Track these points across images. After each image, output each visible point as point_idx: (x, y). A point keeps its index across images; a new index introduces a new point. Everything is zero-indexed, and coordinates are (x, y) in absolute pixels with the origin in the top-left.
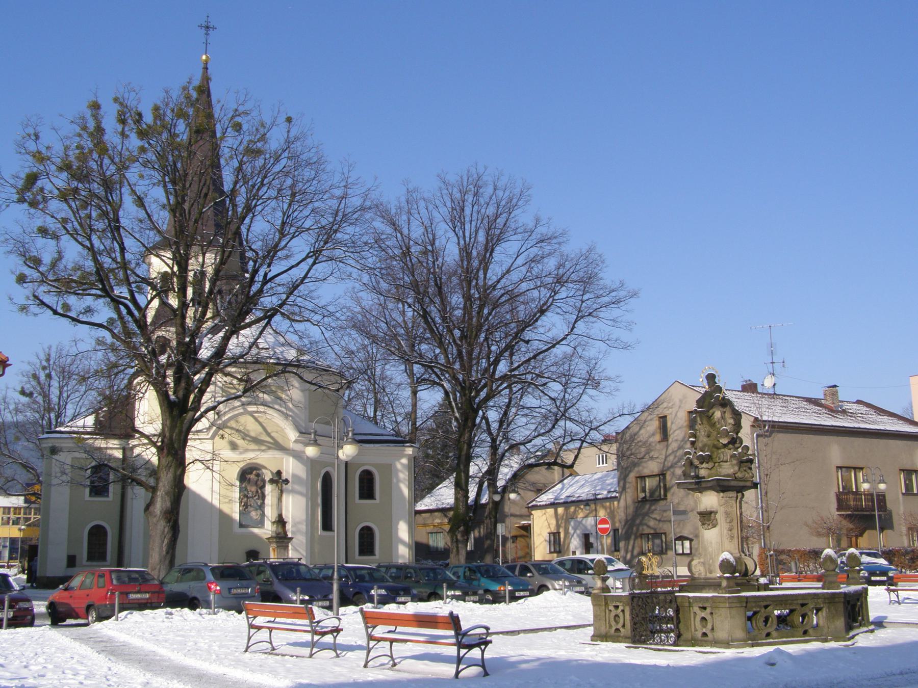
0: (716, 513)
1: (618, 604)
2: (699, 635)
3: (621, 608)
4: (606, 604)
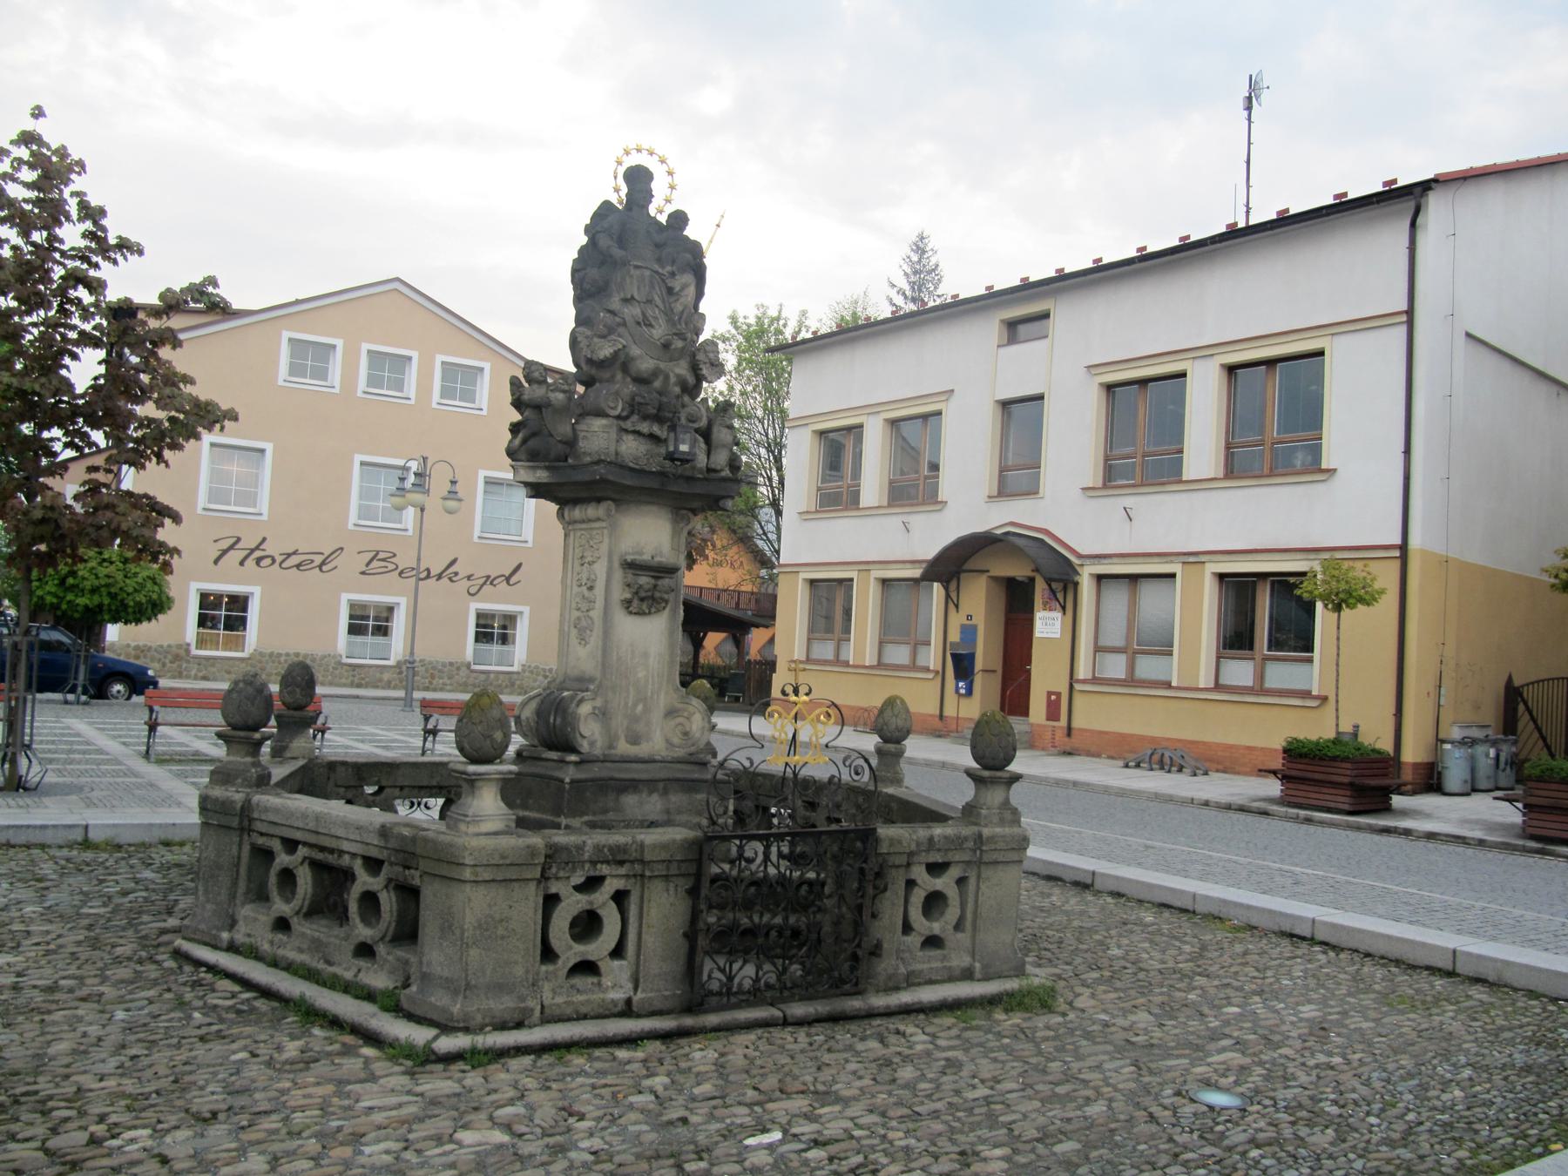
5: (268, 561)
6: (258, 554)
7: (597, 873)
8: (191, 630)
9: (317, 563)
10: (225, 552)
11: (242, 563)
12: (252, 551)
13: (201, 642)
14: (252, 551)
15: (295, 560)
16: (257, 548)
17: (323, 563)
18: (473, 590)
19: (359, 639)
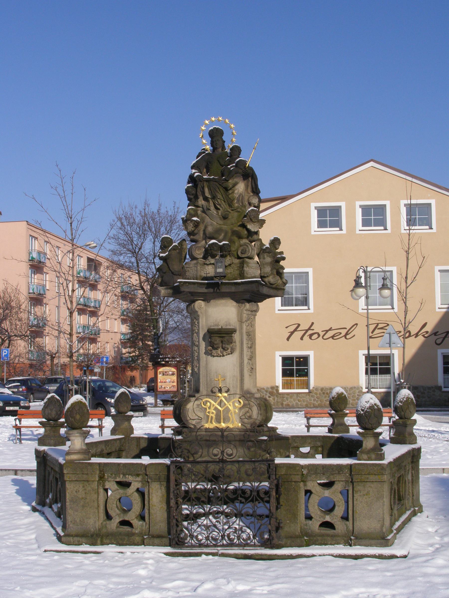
0: (233, 331)
1: (129, 478)
2: (314, 525)
3: (136, 485)
4: (102, 478)
5: (315, 336)
6: (310, 332)
7: (127, 480)
8: (279, 380)
9: (343, 334)
10: (292, 333)
11: (302, 339)
12: (307, 331)
13: (286, 385)
14: (307, 331)
15: (330, 334)
16: (309, 329)
17: (347, 334)
18: (439, 341)
19: (372, 377)
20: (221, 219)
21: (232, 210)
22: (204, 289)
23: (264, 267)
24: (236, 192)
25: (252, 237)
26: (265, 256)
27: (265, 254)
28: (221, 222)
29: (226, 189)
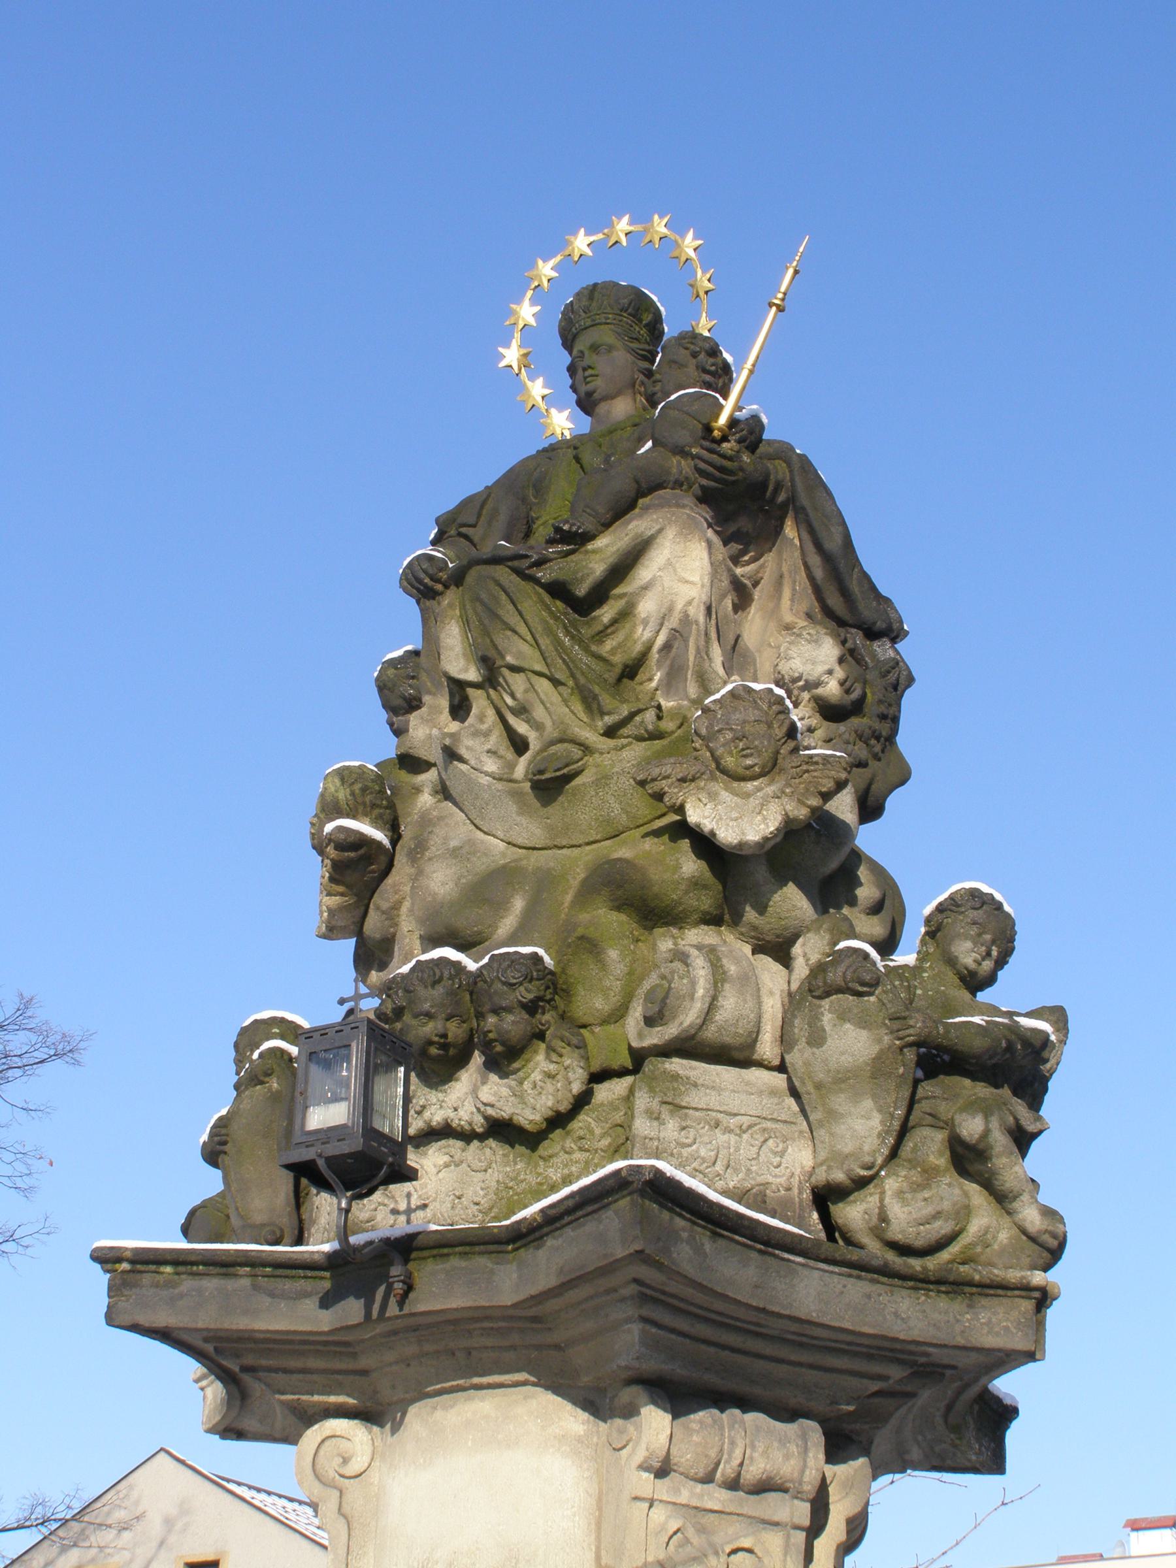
20: (524, 808)
21: (610, 732)
22: (310, 1305)
23: (833, 1115)
24: (647, 607)
25: (762, 909)
26: (827, 1019)
27: (826, 1003)
28: (529, 827)
29: (581, 603)
